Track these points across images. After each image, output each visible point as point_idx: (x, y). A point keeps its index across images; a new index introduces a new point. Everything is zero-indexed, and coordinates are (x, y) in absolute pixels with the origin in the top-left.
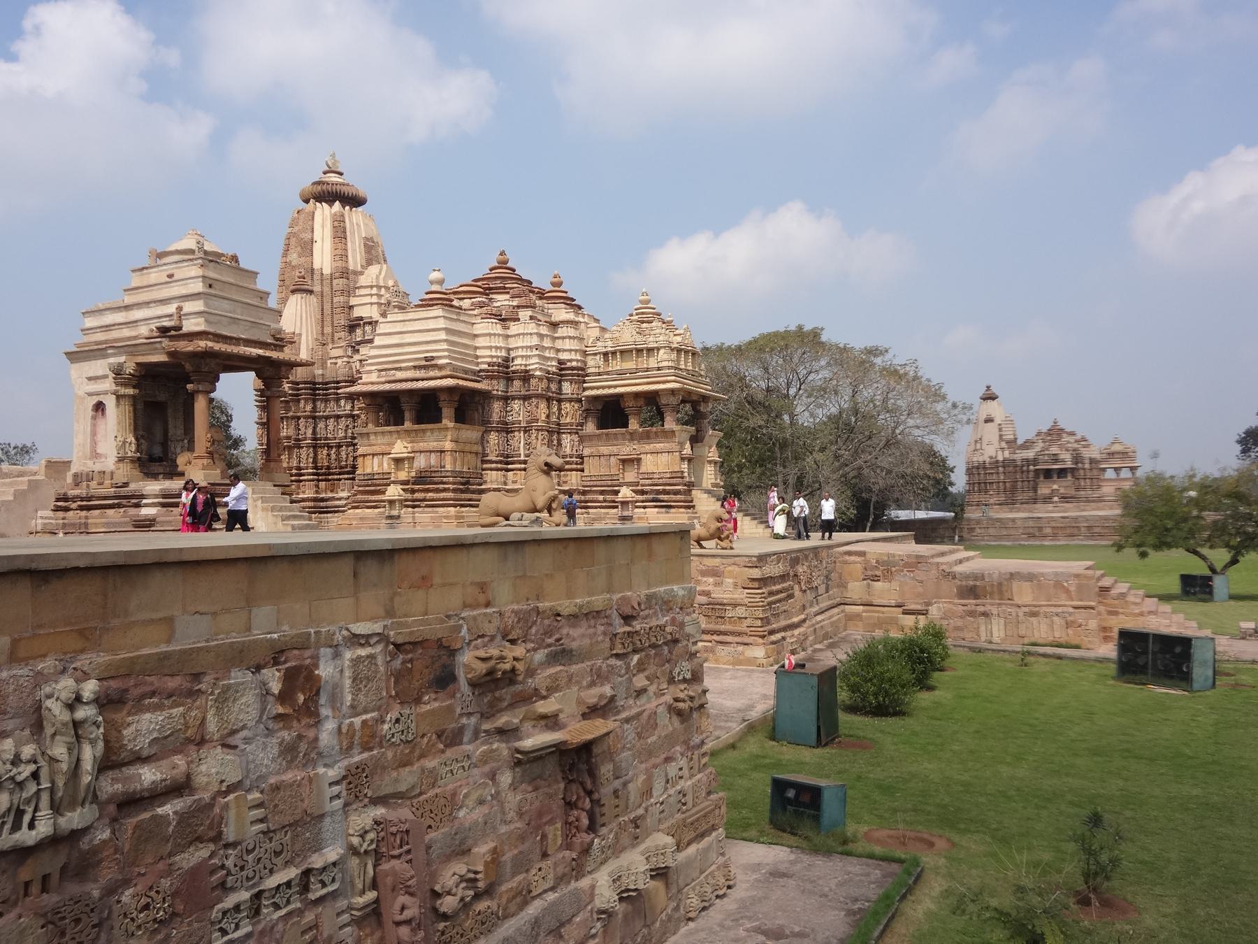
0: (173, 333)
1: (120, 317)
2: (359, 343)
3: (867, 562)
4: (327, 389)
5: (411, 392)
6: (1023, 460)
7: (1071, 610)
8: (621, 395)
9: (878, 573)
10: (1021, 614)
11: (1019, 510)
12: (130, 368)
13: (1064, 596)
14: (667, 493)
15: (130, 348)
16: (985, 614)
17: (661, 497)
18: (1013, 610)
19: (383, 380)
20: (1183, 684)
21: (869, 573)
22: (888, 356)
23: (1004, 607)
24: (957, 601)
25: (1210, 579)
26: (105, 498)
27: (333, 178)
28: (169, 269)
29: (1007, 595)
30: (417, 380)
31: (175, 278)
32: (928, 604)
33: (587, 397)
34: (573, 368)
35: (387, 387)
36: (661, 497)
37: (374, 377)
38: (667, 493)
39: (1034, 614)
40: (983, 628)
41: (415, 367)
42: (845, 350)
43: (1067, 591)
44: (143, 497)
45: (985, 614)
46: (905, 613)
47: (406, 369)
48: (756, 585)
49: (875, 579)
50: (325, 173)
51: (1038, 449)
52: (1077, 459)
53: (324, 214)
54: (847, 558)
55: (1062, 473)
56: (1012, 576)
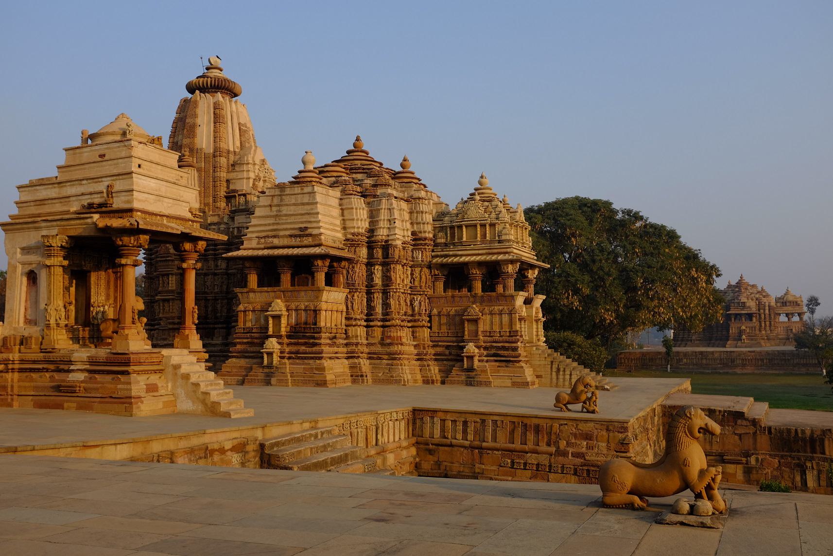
1: (52, 192)
8: (466, 264)
14: (504, 348)
15: (62, 219)
17: (501, 352)
19: (262, 246)
26: (34, 362)
27: (215, 73)
28: (101, 149)
30: (293, 247)
31: (106, 158)
35: (266, 252)
36: (501, 352)
37: (254, 244)
38: (504, 348)
41: (291, 236)
44: (70, 362)
47: (283, 237)
48: (548, 430)
50: (207, 69)
52: (760, 305)
53: (205, 103)
55: (750, 316)
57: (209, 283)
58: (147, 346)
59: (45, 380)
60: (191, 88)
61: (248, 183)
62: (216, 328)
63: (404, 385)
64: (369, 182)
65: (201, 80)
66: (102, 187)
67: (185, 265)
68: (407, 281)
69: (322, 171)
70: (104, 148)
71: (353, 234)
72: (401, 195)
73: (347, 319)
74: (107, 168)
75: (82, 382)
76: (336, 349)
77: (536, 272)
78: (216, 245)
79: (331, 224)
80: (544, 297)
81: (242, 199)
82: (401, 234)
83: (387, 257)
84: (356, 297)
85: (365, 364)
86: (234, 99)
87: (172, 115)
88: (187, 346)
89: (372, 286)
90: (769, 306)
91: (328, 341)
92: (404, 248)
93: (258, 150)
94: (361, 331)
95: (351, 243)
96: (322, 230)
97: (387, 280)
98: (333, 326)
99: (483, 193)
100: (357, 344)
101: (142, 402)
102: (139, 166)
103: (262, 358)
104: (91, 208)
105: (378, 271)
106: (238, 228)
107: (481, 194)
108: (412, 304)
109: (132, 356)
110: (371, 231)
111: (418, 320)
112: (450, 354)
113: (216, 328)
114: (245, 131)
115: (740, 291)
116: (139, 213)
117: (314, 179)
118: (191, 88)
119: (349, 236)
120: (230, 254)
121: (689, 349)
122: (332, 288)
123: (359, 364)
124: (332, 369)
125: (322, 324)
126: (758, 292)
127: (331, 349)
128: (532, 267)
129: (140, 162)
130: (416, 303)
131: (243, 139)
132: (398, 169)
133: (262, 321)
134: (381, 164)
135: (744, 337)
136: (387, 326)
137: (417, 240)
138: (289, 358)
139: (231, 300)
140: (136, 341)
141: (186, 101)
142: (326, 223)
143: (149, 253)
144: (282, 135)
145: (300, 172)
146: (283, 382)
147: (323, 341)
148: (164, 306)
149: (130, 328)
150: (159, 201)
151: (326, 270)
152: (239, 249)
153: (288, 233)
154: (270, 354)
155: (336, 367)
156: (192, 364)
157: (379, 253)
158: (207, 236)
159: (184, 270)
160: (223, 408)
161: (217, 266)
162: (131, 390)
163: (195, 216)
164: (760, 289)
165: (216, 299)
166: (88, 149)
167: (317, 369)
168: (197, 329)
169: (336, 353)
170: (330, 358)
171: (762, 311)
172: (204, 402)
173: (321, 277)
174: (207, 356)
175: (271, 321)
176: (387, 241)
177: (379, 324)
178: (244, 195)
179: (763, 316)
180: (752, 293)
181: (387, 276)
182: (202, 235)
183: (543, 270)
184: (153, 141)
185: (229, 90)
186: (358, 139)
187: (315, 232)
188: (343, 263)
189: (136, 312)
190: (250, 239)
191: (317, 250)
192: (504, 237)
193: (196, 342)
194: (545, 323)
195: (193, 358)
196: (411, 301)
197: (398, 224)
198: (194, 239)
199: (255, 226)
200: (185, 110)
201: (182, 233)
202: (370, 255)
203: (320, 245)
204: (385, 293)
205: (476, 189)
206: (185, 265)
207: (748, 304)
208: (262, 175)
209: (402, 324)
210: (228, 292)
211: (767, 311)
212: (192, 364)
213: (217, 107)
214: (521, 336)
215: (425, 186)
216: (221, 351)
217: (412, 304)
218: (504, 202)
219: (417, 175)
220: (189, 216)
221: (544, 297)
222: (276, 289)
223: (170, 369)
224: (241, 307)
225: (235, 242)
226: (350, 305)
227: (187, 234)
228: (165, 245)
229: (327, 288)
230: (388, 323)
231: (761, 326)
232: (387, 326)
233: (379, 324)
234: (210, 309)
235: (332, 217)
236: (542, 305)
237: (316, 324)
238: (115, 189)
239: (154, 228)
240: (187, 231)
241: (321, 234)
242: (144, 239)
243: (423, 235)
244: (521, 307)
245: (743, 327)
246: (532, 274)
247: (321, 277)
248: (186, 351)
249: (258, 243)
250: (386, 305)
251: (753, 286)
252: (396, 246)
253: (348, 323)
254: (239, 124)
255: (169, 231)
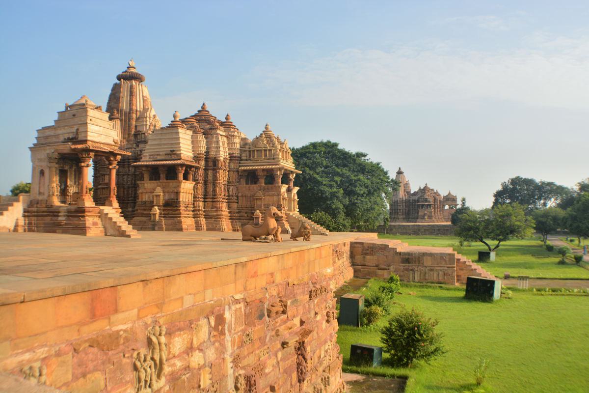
0: (75, 140)
2: (139, 142)
3: (364, 247)
4: (124, 162)
5: (163, 166)
6: (413, 200)
7: (446, 269)
9: (368, 252)
10: (426, 270)
11: (410, 222)
12: (56, 155)
13: (444, 263)
16: (412, 270)
18: (423, 269)
19: (151, 160)
20: (576, 256)
21: (364, 252)
22: (366, 158)
23: (420, 267)
24: (401, 264)
25: (490, 253)
27: (132, 70)
29: (421, 262)
31: (76, 116)
32: (389, 266)
33: (241, 170)
34: (236, 157)
37: (147, 159)
39: (432, 270)
40: (411, 276)
42: (532, 256)
43: (445, 261)
45: (412, 270)
46: (379, 269)
49: (366, 254)
50: (128, 68)
51: (419, 196)
52: (435, 200)
53: (125, 85)
54: (355, 245)
56: (424, 254)
57: (125, 180)
58: (93, 205)
59: (48, 219)
60: (119, 78)
61: (146, 127)
62: (128, 203)
63: (223, 231)
64: (208, 126)
65: (124, 73)
66: (74, 130)
67: (111, 167)
68: (226, 179)
69: (184, 121)
70: (75, 114)
71: (198, 154)
72: (224, 134)
73: (194, 197)
74: (76, 120)
75: (64, 220)
76: (188, 213)
77: (294, 175)
78: (129, 160)
79: (186, 148)
80: (299, 188)
81: (143, 136)
82: (223, 154)
83: (215, 166)
84: (199, 186)
85: (203, 221)
86: (141, 84)
87: (109, 92)
88: (111, 205)
89: (208, 181)
90: (440, 201)
91: (184, 208)
92: (224, 161)
93: (153, 110)
94: (201, 204)
95: (197, 158)
96: (182, 152)
97: (215, 178)
98: (187, 200)
99: (267, 134)
100: (199, 210)
101: (91, 229)
102: (91, 120)
103: (151, 217)
104: (69, 140)
105: (210, 173)
106: (140, 150)
107: (267, 134)
108: (228, 190)
109: (86, 208)
110: (207, 152)
111: (231, 199)
112: (247, 216)
113: (128, 203)
114: (146, 100)
115: (425, 192)
116: (90, 142)
117: (179, 125)
118: (119, 78)
119: (197, 155)
120: (138, 163)
121: (397, 224)
122: (187, 181)
123: (200, 220)
124: (185, 222)
125: (181, 200)
126: (435, 193)
127: (186, 213)
128: (292, 172)
129: (91, 118)
130: (231, 190)
131: (145, 104)
132: (224, 120)
133: (151, 198)
134: (216, 118)
135: (426, 217)
136: (214, 202)
137: (232, 157)
138: (164, 217)
139: (135, 187)
140: (89, 202)
141: (116, 85)
142: (184, 148)
143: (95, 162)
144: (162, 104)
145: (172, 122)
146: (161, 229)
147: (181, 208)
148: (102, 191)
149: (85, 196)
150: (99, 136)
151: (183, 172)
152: (140, 161)
153: (164, 153)
154: (155, 215)
155: (187, 221)
156: (113, 213)
157: (211, 164)
158: (121, 153)
159: (110, 169)
160: (127, 234)
161: (129, 170)
162: (85, 224)
163: (116, 143)
164: (435, 191)
165: (129, 188)
166: (68, 112)
167: (178, 222)
168: (116, 198)
169: (188, 215)
170: (185, 217)
171: (436, 203)
172: (118, 230)
173: (181, 176)
174: (121, 210)
175: (155, 198)
176: (215, 158)
177: (211, 200)
178: (144, 133)
179: (436, 206)
180: (431, 194)
181: (215, 176)
182: (119, 152)
183: (297, 175)
184: (97, 108)
185: (138, 78)
186: (204, 105)
187: (178, 152)
188: (192, 169)
189: (88, 189)
190: (146, 156)
191: (179, 162)
192: (275, 157)
193: (116, 204)
194: (298, 201)
195: (114, 211)
196: (228, 189)
197: (221, 149)
198: (115, 155)
199: (148, 149)
200: (116, 89)
201: (110, 151)
202: (206, 165)
203: (180, 159)
204: (215, 185)
205: (263, 132)
206: (111, 167)
207: (428, 200)
208: (154, 123)
209: (223, 200)
210: (135, 184)
211: (439, 204)
212: (113, 213)
213: (131, 87)
214: (284, 207)
215: (238, 130)
216: (131, 215)
217: (228, 190)
218: (278, 139)
219: (234, 124)
220: (113, 143)
221: (299, 188)
222: (158, 181)
223: (103, 216)
224: (140, 191)
225: (137, 158)
226: (195, 190)
227: (112, 152)
228: (102, 158)
229: (184, 181)
230: (215, 200)
231: (435, 211)
232: (214, 202)
233: (211, 200)
234: (126, 193)
235: (188, 145)
236: (297, 193)
237: (177, 199)
238: (80, 130)
239: (97, 149)
240: (112, 150)
241: (181, 153)
242: (92, 154)
243: (234, 155)
244: (284, 192)
245: (426, 212)
246: (292, 177)
247: (181, 176)
248: (111, 208)
249: (150, 158)
250: (214, 191)
251: (432, 190)
252: (220, 160)
253: (195, 199)
254: (143, 96)
255: (104, 150)
